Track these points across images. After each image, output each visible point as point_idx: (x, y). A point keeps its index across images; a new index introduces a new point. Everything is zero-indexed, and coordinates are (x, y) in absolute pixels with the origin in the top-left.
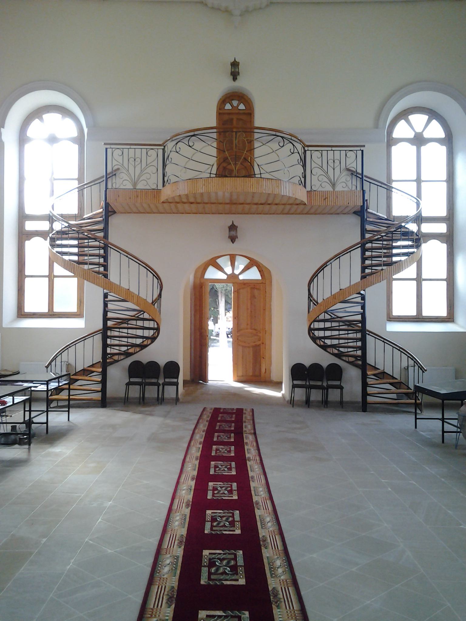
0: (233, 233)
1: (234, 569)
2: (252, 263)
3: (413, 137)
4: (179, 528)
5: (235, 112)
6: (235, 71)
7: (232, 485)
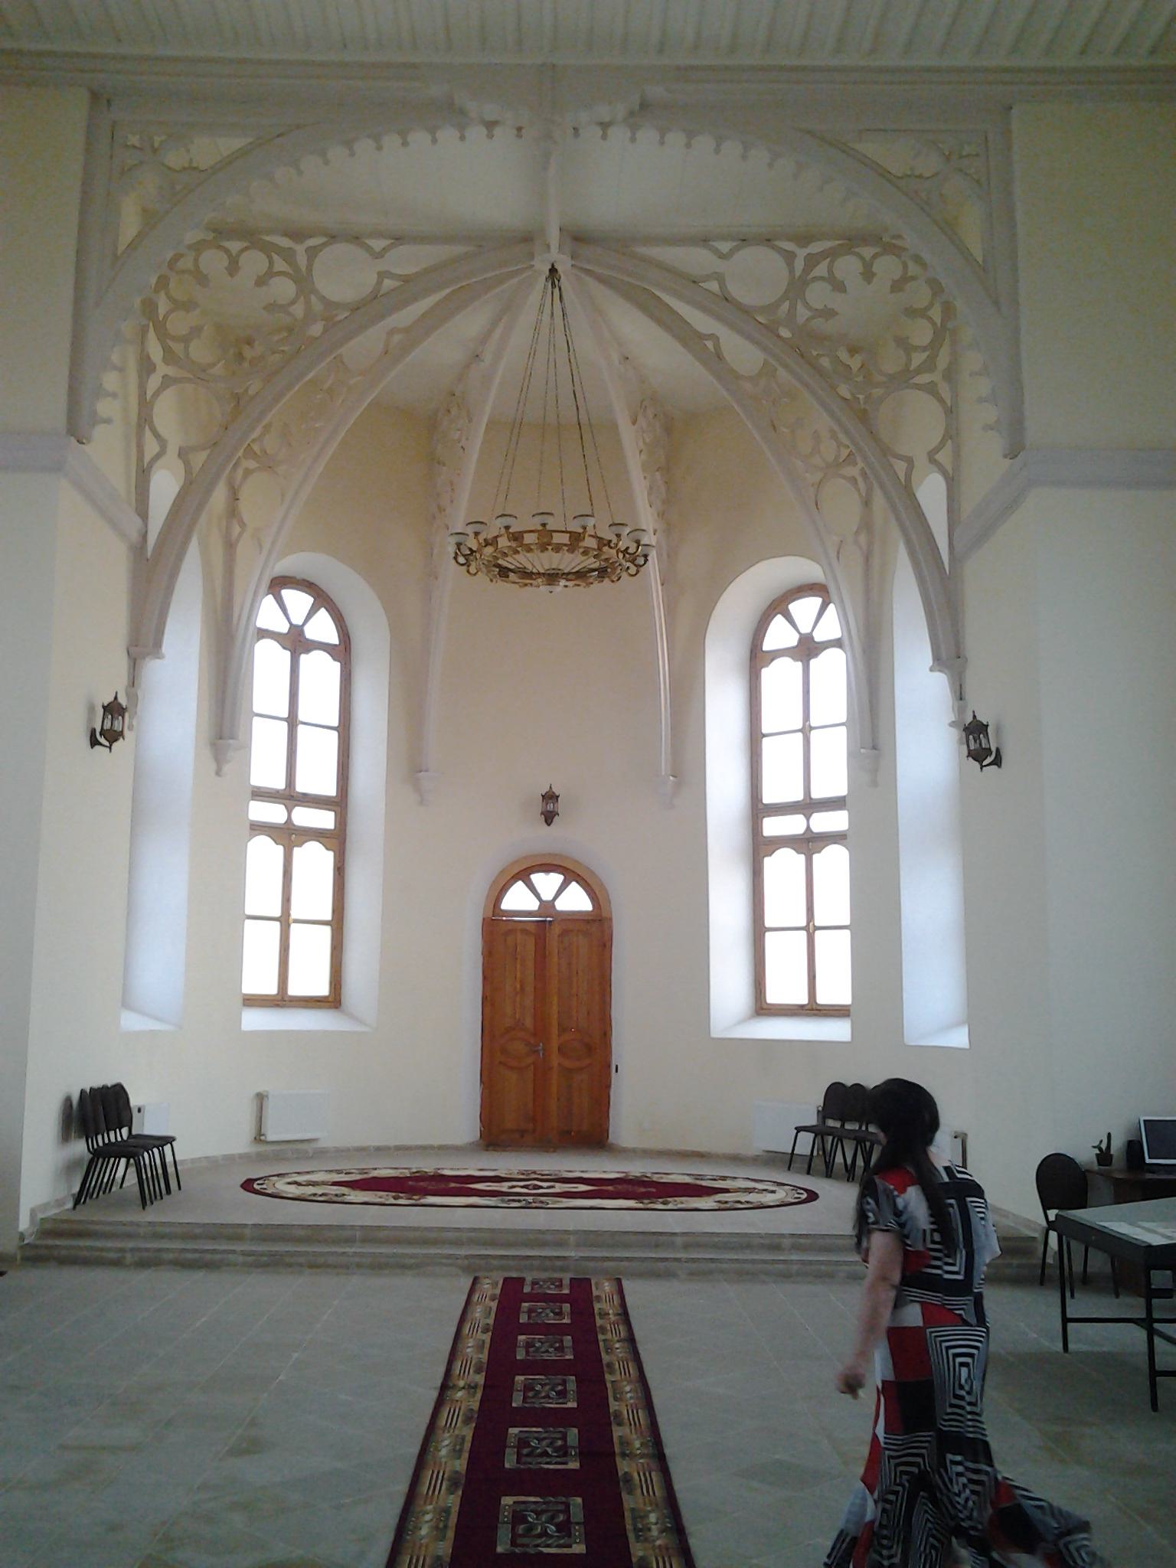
0: (550, 807)
1: (563, 1451)
2: (572, 874)
3: (795, 643)
4: (451, 1458)
5: (548, 923)
6: (549, 808)
7: (568, 1506)
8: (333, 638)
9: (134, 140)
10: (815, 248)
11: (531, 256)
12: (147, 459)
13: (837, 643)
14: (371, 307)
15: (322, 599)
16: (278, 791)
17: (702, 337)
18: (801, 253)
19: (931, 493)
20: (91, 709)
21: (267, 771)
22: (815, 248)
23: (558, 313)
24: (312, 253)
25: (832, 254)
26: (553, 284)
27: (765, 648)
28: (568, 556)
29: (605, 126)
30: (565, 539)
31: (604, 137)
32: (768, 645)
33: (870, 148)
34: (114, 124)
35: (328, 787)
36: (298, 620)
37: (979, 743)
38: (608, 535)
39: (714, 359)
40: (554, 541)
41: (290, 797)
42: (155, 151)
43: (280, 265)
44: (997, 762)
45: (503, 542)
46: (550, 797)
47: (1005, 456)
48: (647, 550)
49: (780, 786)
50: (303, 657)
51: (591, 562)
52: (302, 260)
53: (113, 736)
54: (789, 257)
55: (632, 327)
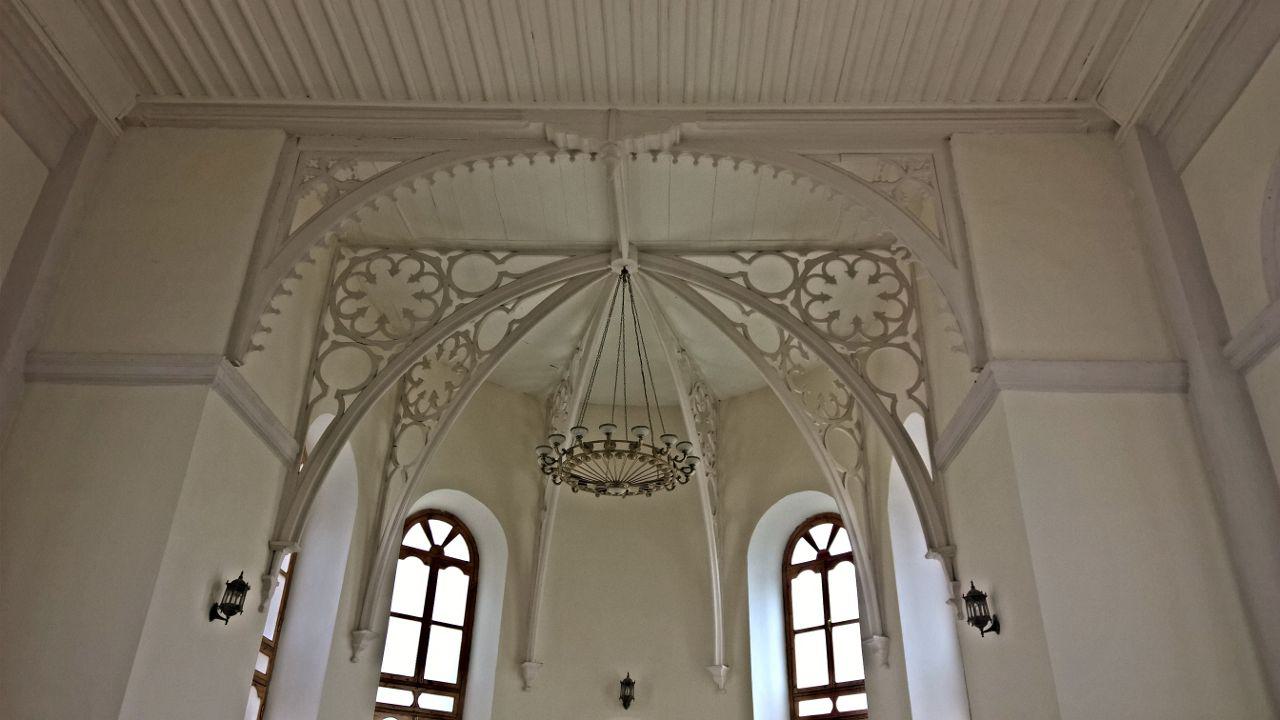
0: (628, 692)
8: (465, 556)
9: (314, 163)
10: (812, 256)
11: (609, 262)
12: (311, 398)
13: (848, 557)
14: (494, 296)
15: (459, 527)
16: (408, 678)
17: (735, 325)
18: (802, 260)
19: (914, 425)
20: (216, 587)
21: (399, 658)
22: (812, 256)
23: (627, 289)
24: (452, 261)
25: (825, 260)
26: (625, 281)
27: (793, 563)
28: (629, 462)
29: (654, 152)
30: (625, 447)
31: (655, 160)
32: (796, 559)
33: (846, 165)
34: (301, 153)
35: (450, 676)
36: (439, 541)
37: (977, 610)
38: (660, 445)
39: (744, 340)
40: (617, 448)
41: (418, 683)
42: (328, 169)
43: (428, 267)
44: (996, 628)
45: (578, 451)
46: (628, 683)
47: (973, 371)
48: (693, 461)
49: (811, 674)
50: (441, 571)
51: (650, 472)
52: (445, 264)
53: (232, 610)
54: (794, 263)
55: (686, 321)
